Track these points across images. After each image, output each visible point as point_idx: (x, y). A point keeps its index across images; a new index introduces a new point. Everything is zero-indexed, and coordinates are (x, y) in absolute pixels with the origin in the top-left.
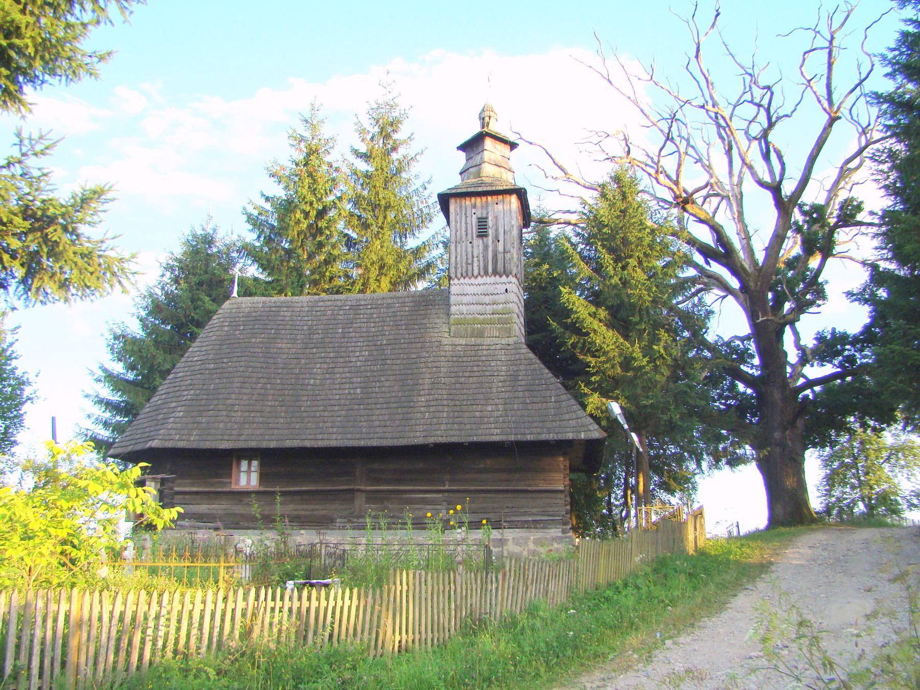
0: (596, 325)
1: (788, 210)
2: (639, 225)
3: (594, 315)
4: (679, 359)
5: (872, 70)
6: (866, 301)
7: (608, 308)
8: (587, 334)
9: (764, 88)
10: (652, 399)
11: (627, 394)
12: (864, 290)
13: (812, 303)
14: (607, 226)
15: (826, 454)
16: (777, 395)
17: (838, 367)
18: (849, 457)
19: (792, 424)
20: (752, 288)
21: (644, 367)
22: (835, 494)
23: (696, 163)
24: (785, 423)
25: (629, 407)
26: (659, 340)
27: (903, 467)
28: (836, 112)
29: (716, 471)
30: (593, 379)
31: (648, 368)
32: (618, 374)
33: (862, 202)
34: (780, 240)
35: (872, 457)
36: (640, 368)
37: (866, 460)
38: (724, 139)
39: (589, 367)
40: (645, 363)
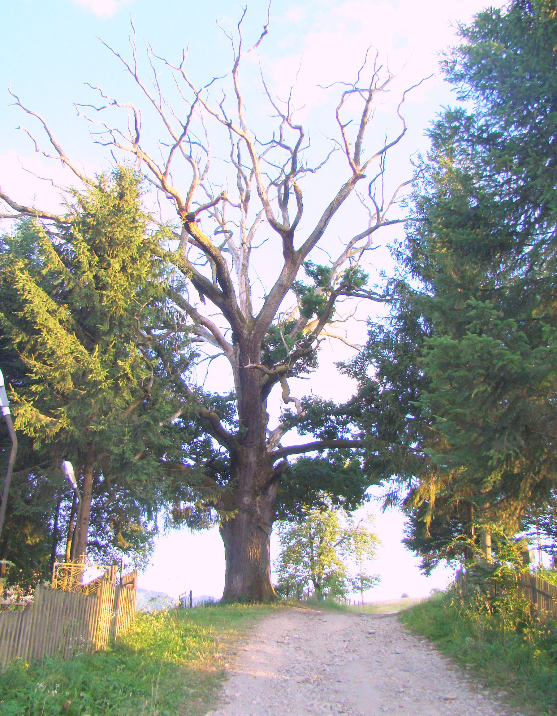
0: (52, 323)
1: (296, 261)
2: (130, 223)
3: (52, 313)
4: (149, 390)
5: (403, 134)
6: (356, 375)
7: (74, 311)
8: (39, 332)
9: (296, 128)
10: (104, 424)
11: (74, 413)
12: (356, 363)
13: (300, 368)
14: (93, 216)
15: (285, 531)
16: (252, 458)
18: (305, 536)
19: (264, 490)
20: (245, 336)
21: (100, 382)
22: (289, 570)
23: (210, 217)
24: (257, 488)
25: (73, 431)
26: (126, 355)
27: (352, 551)
28: (361, 171)
29: (172, 530)
30: (34, 388)
31: (104, 385)
33: (366, 276)
34: (282, 290)
35: (328, 538)
36: (96, 383)
38: (243, 191)
39: (32, 372)
40: (101, 377)
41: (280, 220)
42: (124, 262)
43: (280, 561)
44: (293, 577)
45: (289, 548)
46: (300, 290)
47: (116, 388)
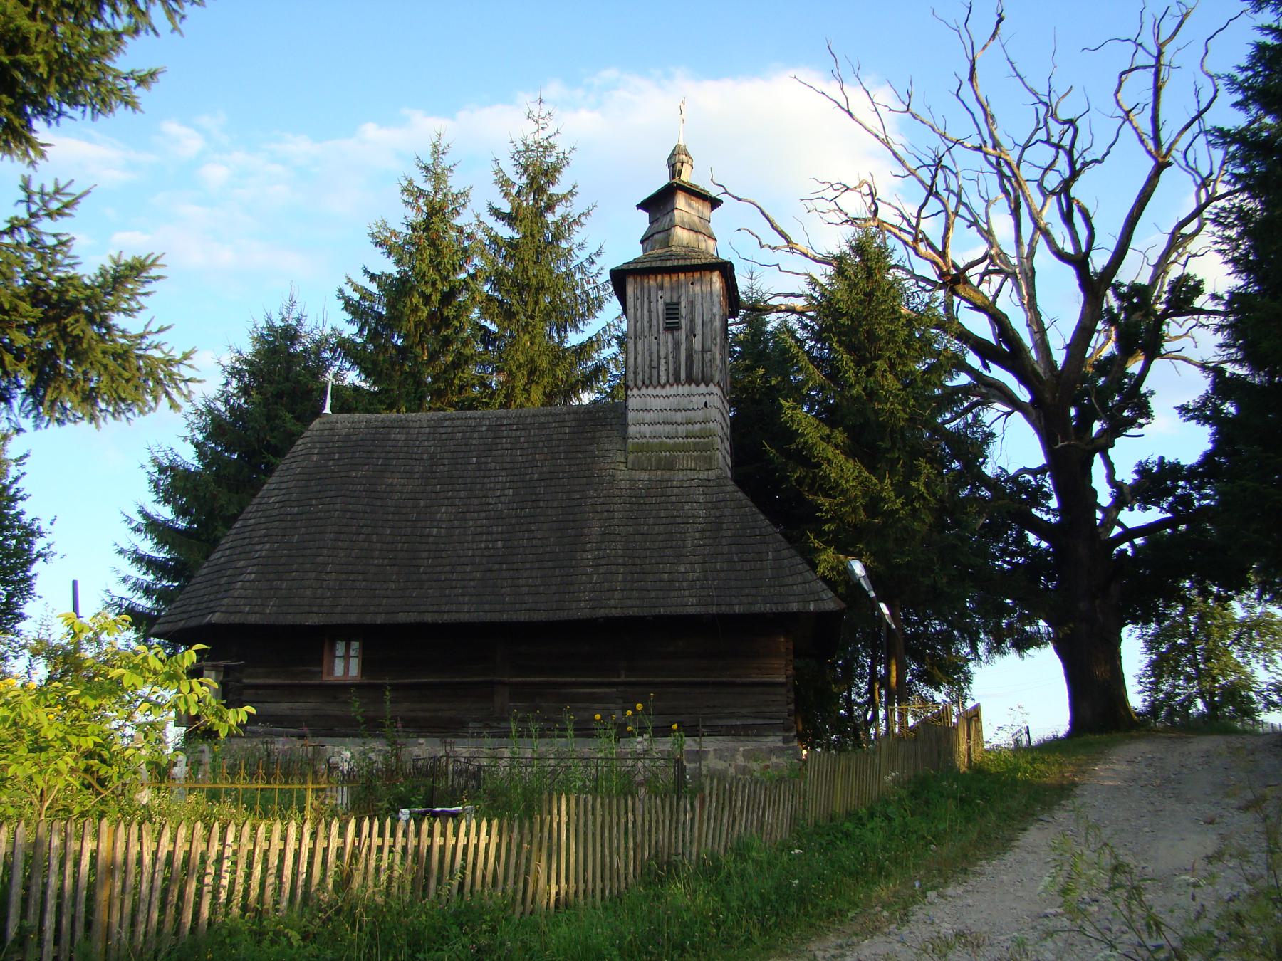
0: (830, 452)
2: (890, 314)
3: (827, 439)
8: (818, 465)
9: (1065, 122)
12: (1204, 403)
14: (846, 314)
15: (1150, 632)
17: (1167, 512)
18: (1182, 637)
21: (897, 511)
23: (969, 227)
28: (1165, 156)
30: (826, 527)
32: (861, 520)
33: (1201, 282)
36: (893, 512)
37: (1207, 641)
39: (821, 511)
40: (898, 506)
41: (1069, 249)
42: (890, 359)
43: (1149, 677)
44: (1169, 696)
45: (1160, 655)
46: (1112, 320)
47: (914, 512)
